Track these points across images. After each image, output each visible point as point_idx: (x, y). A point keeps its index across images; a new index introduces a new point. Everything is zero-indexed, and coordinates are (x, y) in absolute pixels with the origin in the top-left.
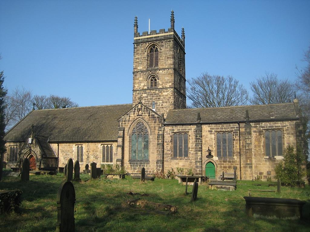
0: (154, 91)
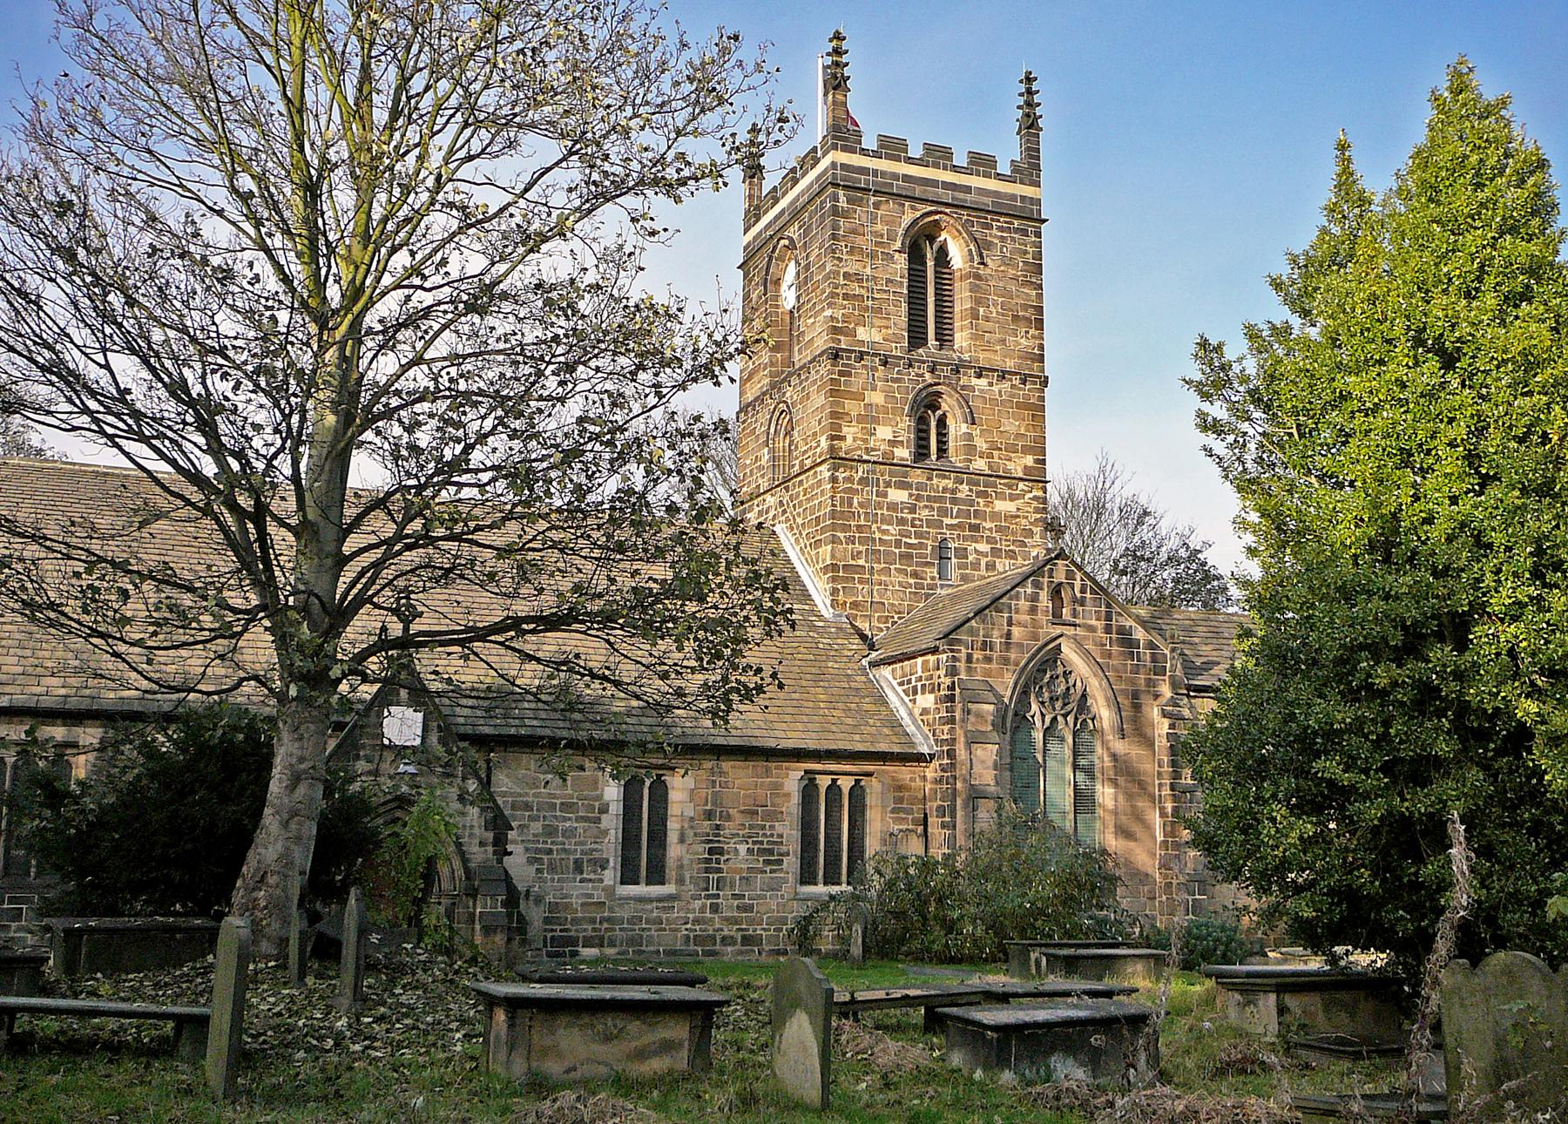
0: (950, 484)
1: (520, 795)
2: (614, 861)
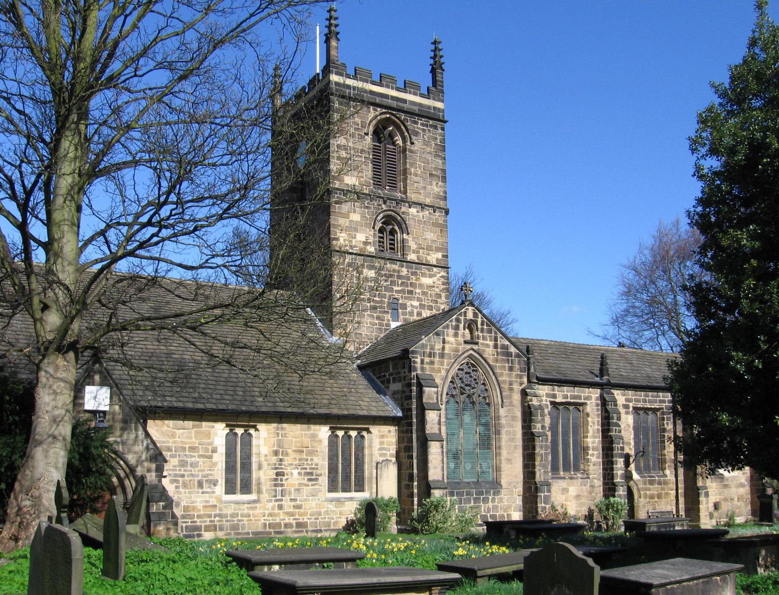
1: (164, 442)
2: (222, 482)
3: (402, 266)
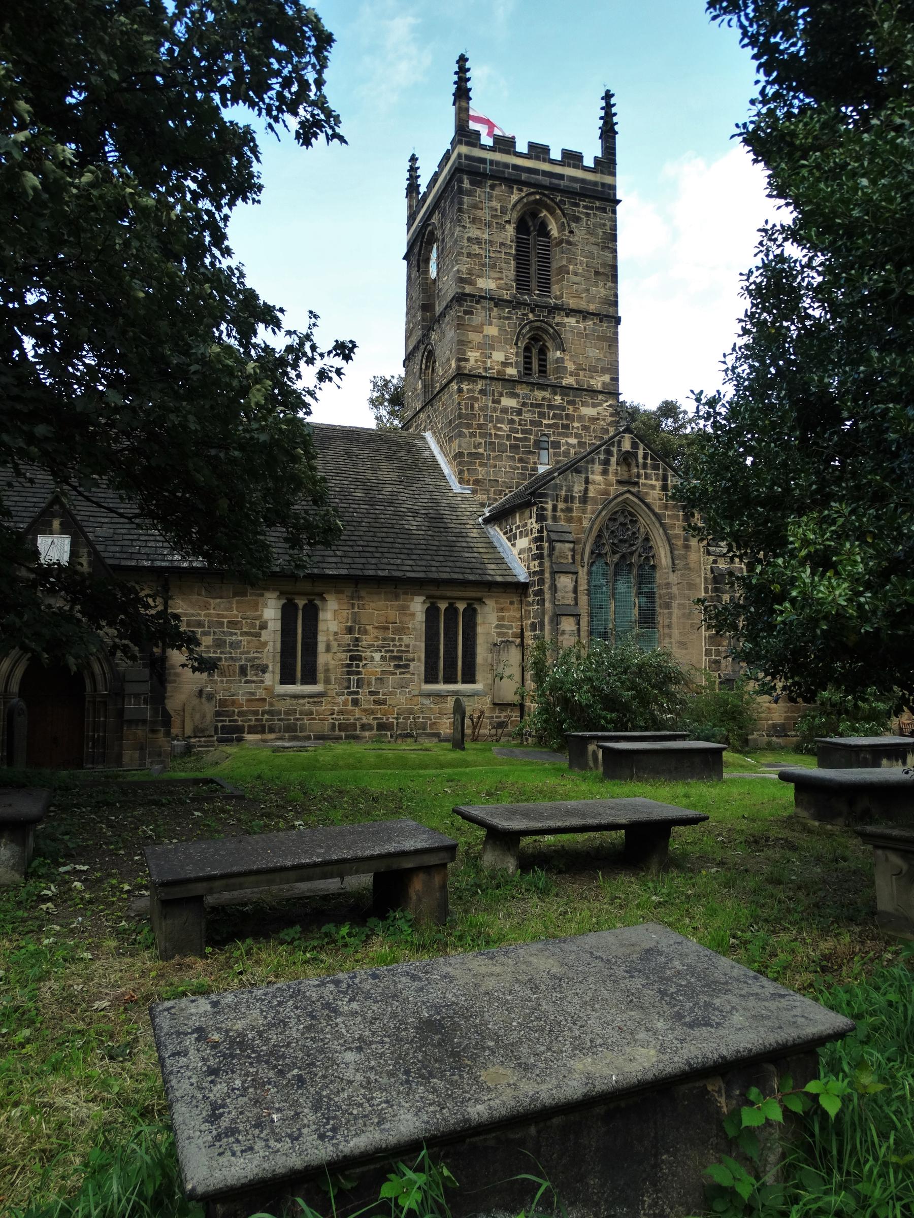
1: (193, 615)
3: (556, 394)
